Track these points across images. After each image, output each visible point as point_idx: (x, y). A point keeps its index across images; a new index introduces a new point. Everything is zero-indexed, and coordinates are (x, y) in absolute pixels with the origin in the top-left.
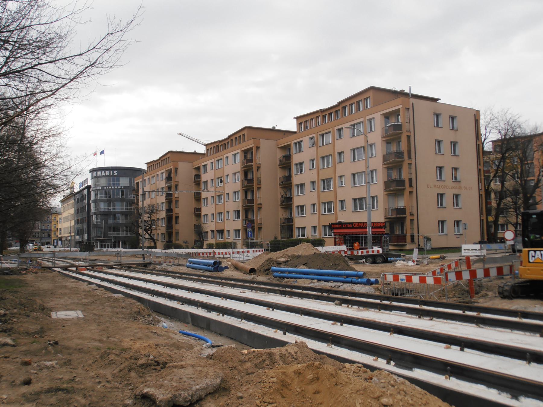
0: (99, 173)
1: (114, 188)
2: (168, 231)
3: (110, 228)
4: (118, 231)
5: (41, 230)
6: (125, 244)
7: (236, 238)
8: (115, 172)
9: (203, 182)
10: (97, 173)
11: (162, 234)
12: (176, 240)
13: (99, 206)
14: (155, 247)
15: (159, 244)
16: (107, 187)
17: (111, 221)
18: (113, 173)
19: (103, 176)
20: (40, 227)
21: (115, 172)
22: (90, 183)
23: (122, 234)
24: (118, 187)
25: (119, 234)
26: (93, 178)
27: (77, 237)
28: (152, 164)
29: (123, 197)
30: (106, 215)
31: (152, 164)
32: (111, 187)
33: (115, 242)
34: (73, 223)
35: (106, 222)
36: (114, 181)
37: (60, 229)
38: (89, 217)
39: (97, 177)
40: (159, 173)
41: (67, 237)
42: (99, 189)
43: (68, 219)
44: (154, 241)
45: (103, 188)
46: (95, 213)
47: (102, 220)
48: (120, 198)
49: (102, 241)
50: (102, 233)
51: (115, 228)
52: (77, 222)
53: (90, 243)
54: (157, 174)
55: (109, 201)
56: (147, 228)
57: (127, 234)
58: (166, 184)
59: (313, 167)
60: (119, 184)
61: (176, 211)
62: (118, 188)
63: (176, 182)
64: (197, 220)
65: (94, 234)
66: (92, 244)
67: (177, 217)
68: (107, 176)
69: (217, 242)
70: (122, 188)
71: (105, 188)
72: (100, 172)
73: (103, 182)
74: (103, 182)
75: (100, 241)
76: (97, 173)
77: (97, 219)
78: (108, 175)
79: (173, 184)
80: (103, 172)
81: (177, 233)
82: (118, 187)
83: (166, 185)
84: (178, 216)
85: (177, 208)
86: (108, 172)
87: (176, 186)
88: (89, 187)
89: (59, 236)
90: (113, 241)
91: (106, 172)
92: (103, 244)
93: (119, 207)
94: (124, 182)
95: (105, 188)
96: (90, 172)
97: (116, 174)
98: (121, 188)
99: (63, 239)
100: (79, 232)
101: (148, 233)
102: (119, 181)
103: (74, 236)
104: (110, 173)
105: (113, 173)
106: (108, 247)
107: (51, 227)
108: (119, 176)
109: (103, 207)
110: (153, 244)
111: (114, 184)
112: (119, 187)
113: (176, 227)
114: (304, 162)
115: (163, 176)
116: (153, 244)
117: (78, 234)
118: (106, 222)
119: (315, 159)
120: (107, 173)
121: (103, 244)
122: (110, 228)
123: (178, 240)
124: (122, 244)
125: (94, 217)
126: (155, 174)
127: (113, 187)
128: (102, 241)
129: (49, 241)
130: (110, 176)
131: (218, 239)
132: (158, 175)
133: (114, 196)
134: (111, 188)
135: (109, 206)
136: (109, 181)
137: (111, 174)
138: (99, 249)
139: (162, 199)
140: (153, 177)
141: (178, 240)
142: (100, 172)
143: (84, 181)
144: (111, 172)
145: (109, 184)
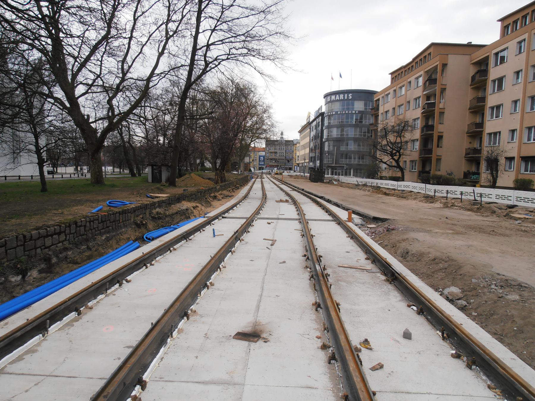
0: (333, 97)
1: (348, 112)
2: (422, 157)
3: (342, 155)
4: (350, 158)
5: (285, 157)
6: (357, 172)
7: (412, 169)
8: (350, 95)
9: (492, 81)
10: (331, 98)
11: (412, 161)
12: (436, 170)
13: (331, 132)
14: (402, 179)
15: (407, 175)
16: (340, 111)
17: (343, 148)
18: (348, 97)
19: (337, 101)
20: (284, 155)
21: (350, 95)
22: (324, 110)
23: (354, 161)
24: (352, 111)
25: (350, 161)
26: (327, 103)
27: (311, 164)
28: (400, 72)
29: (357, 122)
30: (338, 141)
31: (400, 72)
32: (345, 111)
33: (347, 169)
34: (307, 150)
35: (338, 149)
36: (348, 105)
37: (298, 156)
38: (322, 144)
39: (331, 102)
40: (412, 79)
41: (302, 163)
42: (333, 115)
43: (304, 147)
44: (402, 170)
45: (336, 113)
46: (327, 140)
47: (334, 146)
48: (354, 123)
49: (333, 168)
50: (333, 160)
51: (347, 155)
52: (311, 150)
53: (322, 169)
54: (409, 80)
55: (341, 126)
56: (394, 152)
57: (359, 162)
58: (423, 91)
59: (515, 110)
60: (353, 109)
61: (439, 128)
62: (352, 112)
63: (442, 85)
64: (470, 143)
65: (325, 161)
66: (324, 171)
67: (440, 138)
68: (342, 100)
69: (519, 178)
70: (357, 112)
71: (339, 113)
72: (334, 96)
73: (337, 107)
74: (337, 107)
75: (331, 168)
76: (331, 98)
77: (329, 146)
78: (343, 98)
79: (438, 88)
80: (337, 96)
81: (439, 160)
82: (352, 111)
83: (424, 93)
84: (442, 136)
85: (440, 123)
86: (343, 95)
87: (443, 90)
88: (322, 114)
89: (297, 162)
90: (345, 168)
91: (341, 95)
92: (334, 171)
93: (351, 133)
94: (359, 106)
95: (339, 113)
96: (324, 98)
97: (350, 98)
98: (355, 113)
99: (300, 165)
100: (312, 159)
101: (394, 159)
102: (353, 105)
103: (309, 162)
104: (344, 97)
105: (348, 97)
106: (339, 175)
107: (293, 155)
108: (354, 99)
109: (335, 133)
110: (399, 174)
111: (348, 109)
112: (354, 112)
113: (437, 152)
114: (502, 105)
115: (418, 82)
116: (399, 174)
117: (311, 161)
118: (338, 149)
119: (519, 100)
120: (342, 96)
121: (334, 171)
122: (342, 155)
123: (439, 170)
124: (354, 172)
125: (327, 144)
126: (405, 83)
127: (347, 112)
128: (333, 168)
129: (291, 167)
130: (344, 100)
131: (522, 171)
132: (410, 82)
133: (348, 122)
134: (345, 113)
135: (342, 131)
136: (343, 106)
137: (346, 98)
138: (330, 176)
139: (418, 113)
140: (401, 88)
141: (439, 170)
142: (334, 96)
143: (319, 109)
144: (346, 95)
145: (344, 109)
